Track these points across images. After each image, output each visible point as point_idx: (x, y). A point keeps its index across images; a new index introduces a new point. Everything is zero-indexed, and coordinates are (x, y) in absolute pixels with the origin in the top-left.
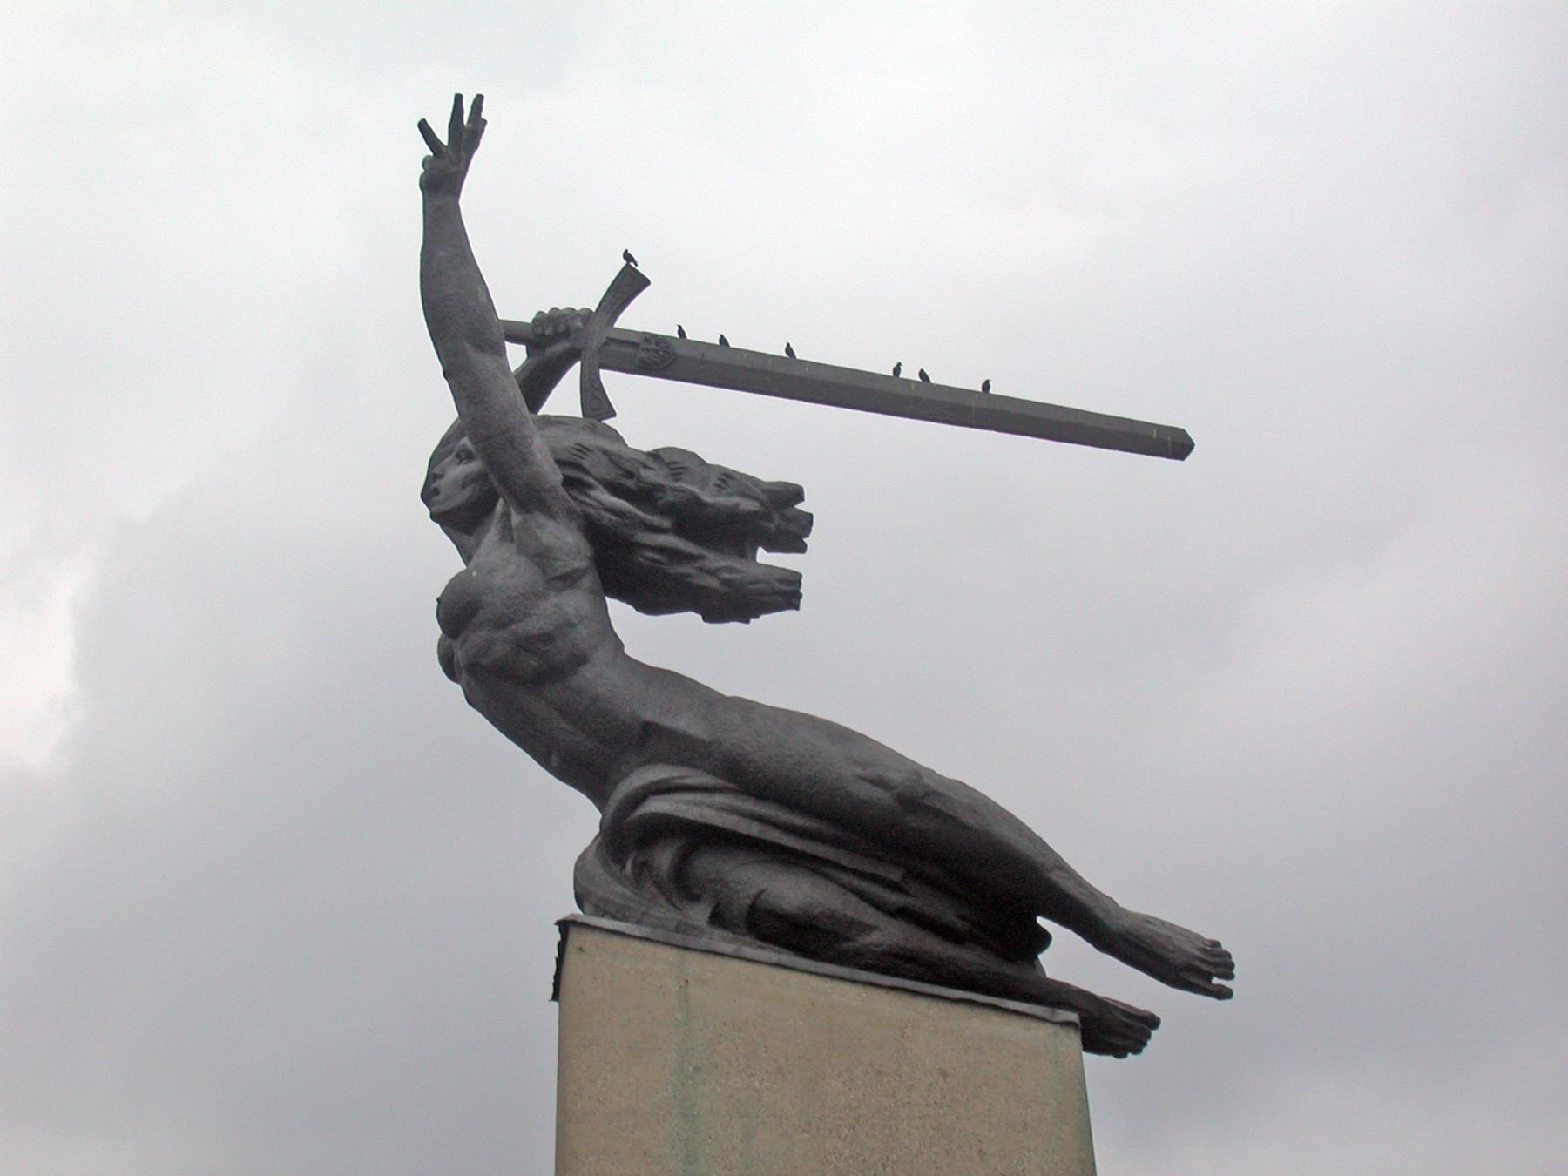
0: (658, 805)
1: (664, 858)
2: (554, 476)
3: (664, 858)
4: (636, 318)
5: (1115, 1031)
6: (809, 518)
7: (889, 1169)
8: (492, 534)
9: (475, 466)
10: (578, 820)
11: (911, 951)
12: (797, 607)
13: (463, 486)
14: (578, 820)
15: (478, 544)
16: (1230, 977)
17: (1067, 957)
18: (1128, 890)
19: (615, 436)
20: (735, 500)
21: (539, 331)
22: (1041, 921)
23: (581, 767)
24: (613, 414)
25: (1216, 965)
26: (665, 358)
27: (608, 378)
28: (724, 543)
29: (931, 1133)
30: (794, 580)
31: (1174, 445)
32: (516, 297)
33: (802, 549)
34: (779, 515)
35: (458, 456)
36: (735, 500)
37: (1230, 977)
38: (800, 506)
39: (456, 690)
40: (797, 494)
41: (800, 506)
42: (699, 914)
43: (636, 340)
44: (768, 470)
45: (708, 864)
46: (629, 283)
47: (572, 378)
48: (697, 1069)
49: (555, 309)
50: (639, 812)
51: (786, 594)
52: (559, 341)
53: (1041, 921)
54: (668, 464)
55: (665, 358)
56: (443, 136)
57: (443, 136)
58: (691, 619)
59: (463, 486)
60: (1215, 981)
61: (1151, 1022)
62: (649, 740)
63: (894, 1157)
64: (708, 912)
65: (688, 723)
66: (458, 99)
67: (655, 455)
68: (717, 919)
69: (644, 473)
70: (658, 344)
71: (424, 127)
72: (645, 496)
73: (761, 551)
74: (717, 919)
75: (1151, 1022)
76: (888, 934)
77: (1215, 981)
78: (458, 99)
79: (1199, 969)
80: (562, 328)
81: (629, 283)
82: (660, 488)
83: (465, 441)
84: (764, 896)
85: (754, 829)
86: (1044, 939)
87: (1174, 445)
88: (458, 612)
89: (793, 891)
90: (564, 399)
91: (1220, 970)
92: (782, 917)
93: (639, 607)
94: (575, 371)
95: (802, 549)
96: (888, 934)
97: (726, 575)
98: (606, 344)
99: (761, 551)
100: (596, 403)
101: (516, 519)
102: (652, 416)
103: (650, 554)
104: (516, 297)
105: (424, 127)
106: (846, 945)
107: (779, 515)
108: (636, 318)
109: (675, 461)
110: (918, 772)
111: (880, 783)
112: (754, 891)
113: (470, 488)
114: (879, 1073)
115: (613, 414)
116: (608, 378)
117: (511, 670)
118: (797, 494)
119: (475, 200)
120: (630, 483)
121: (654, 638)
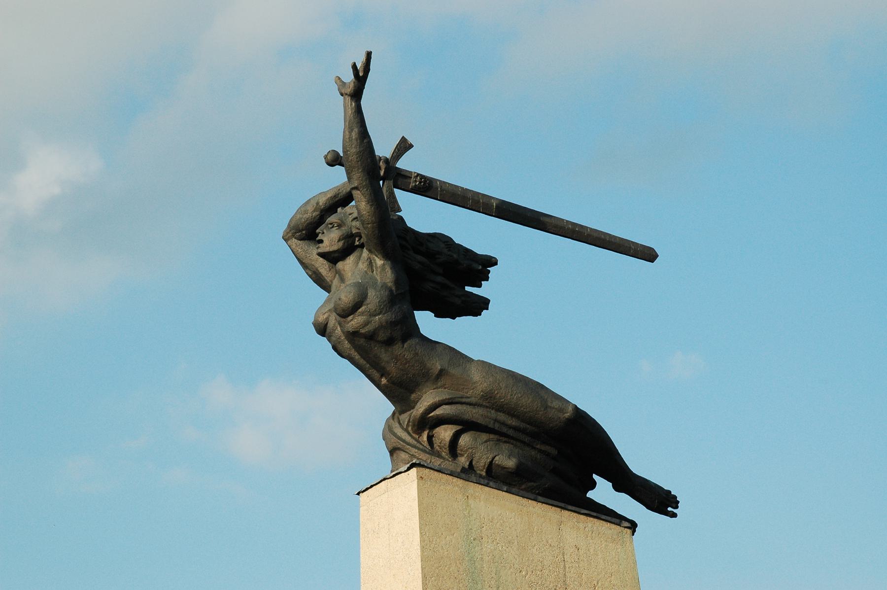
1: (445, 433)
3: (445, 433)
11: (432, 404)
16: (677, 507)
17: (603, 492)
18: (638, 464)
26: (426, 187)
28: (449, 278)
31: (648, 255)
34: (479, 267)
37: (677, 507)
40: (487, 279)
48: (474, 539)
51: (478, 306)
55: (426, 187)
59: (339, 241)
60: (670, 509)
72: (431, 255)
77: (670, 509)
79: (661, 501)
86: (593, 485)
87: (648, 255)
95: (480, 286)
106: (393, 288)
107: (479, 267)
108: (403, 164)
117: (381, 347)
118: (487, 279)
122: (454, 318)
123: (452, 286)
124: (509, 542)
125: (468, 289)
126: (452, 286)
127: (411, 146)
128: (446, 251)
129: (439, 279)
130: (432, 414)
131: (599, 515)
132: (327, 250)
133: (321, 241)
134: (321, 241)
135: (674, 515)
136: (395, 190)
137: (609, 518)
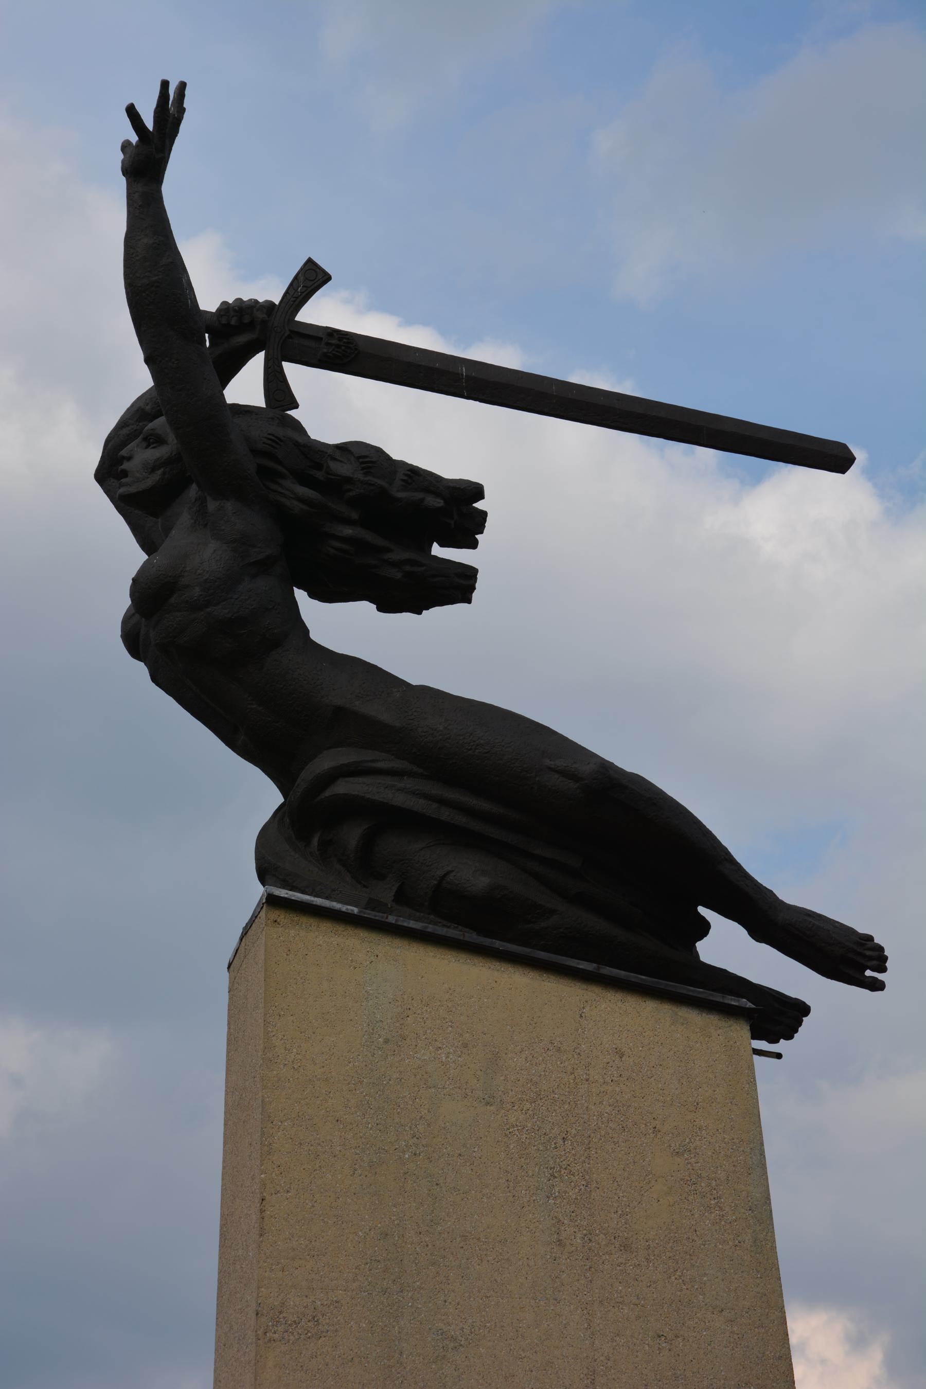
0: (342, 787)
1: (352, 836)
3: (352, 836)
5: (778, 1017)
6: (483, 515)
7: (568, 1143)
8: (184, 518)
9: (162, 452)
10: (262, 796)
12: (469, 601)
13: (153, 469)
14: (262, 796)
15: (167, 530)
16: (883, 969)
17: (727, 945)
19: (297, 426)
20: (419, 495)
21: (224, 321)
22: (702, 910)
24: (295, 405)
25: (871, 958)
27: (293, 372)
28: (411, 536)
29: (608, 1109)
32: (213, 286)
33: (473, 545)
34: (457, 509)
35: (145, 439)
36: (419, 495)
37: (883, 969)
38: (479, 505)
39: (140, 670)
40: (477, 492)
41: (479, 505)
42: (386, 892)
43: (320, 335)
44: (449, 468)
46: (311, 279)
47: (256, 366)
48: (386, 1041)
49: (239, 300)
50: (328, 793)
51: (458, 586)
52: (272, 330)
53: (702, 910)
54: (358, 458)
56: (149, 122)
57: (149, 122)
58: (366, 608)
60: (868, 973)
61: (802, 1009)
62: (344, 724)
63: (574, 1131)
64: (395, 889)
66: (165, 85)
67: (345, 449)
68: (402, 898)
69: (333, 465)
70: (340, 339)
71: (132, 112)
72: (334, 486)
73: (435, 545)
74: (402, 898)
75: (802, 1009)
77: (868, 973)
78: (165, 85)
79: (850, 958)
80: (246, 320)
82: (349, 480)
83: (160, 422)
84: (451, 877)
85: (446, 815)
86: (704, 928)
88: (149, 595)
89: (472, 873)
90: (246, 387)
91: (874, 963)
94: (259, 360)
95: (473, 545)
97: (408, 568)
98: (289, 337)
99: (435, 545)
100: (279, 393)
101: (212, 505)
102: (336, 409)
103: (337, 544)
104: (213, 286)
105: (132, 112)
107: (457, 509)
108: (318, 312)
109: (367, 458)
110: (606, 767)
111: (572, 776)
112: (440, 873)
113: (160, 472)
114: (559, 1050)
115: (295, 405)
116: (293, 372)
117: (208, 646)
118: (477, 492)
119: (181, 186)
120: (320, 475)
121: (342, 626)
122: (419, 612)
123: (380, 542)
124: (465, 1045)
125: (437, 550)
126: (380, 542)
127: (327, 278)
128: (359, 476)
129: (348, 531)
130: (322, 796)
131: (663, 984)
132: (133, 489)
133: (125, 474)
134: (125, 474)
135: (877, 986)
136: (286, 365)
137: (699, 992)
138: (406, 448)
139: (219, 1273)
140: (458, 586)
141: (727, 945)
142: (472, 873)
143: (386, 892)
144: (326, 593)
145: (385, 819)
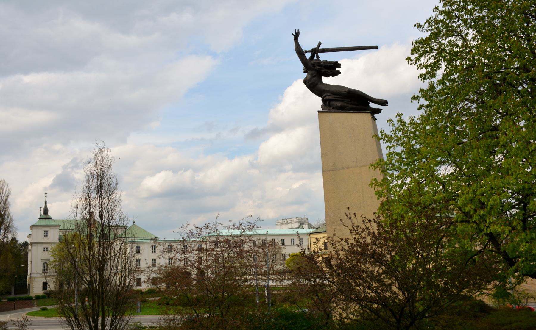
2: (312, 66)
3: (327, 103)
4: (321, 47)
17: (372, 105)
23: (319, 95)
26: (324, 51)
28: (332, 69)
30: (339, 71)
31: (376, 47)
40: (337, 62)
42: (331, 108)
45: (332, 103)
46: (320, 44)
51: (339, 73)
52: (315, 51)
55: (324, 51)
65: (327, 89)
68: (333, 108)
74: (333, 108)
76: (350, 106)
79: (384, 103)
81: (320, 44)
87: (376, 47)
89: (339, 104)
92: (338, 107)
93: (333, 76)
96: (350, 106)
100: (318, 57)
102: (323, 57)
108: (321, 47)
109: (325, 62)
117: (314, 85)
119: (300, 40)
121: (326, 80)
138: (329, 60)
139: (322, 157)
140: (339, 73)
141: (372, 105)
142: (339, 104)
143: (331, 108)
144: (327, 76)
145: (330, 100)
